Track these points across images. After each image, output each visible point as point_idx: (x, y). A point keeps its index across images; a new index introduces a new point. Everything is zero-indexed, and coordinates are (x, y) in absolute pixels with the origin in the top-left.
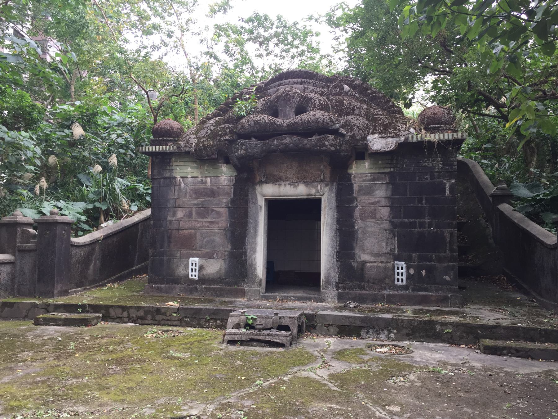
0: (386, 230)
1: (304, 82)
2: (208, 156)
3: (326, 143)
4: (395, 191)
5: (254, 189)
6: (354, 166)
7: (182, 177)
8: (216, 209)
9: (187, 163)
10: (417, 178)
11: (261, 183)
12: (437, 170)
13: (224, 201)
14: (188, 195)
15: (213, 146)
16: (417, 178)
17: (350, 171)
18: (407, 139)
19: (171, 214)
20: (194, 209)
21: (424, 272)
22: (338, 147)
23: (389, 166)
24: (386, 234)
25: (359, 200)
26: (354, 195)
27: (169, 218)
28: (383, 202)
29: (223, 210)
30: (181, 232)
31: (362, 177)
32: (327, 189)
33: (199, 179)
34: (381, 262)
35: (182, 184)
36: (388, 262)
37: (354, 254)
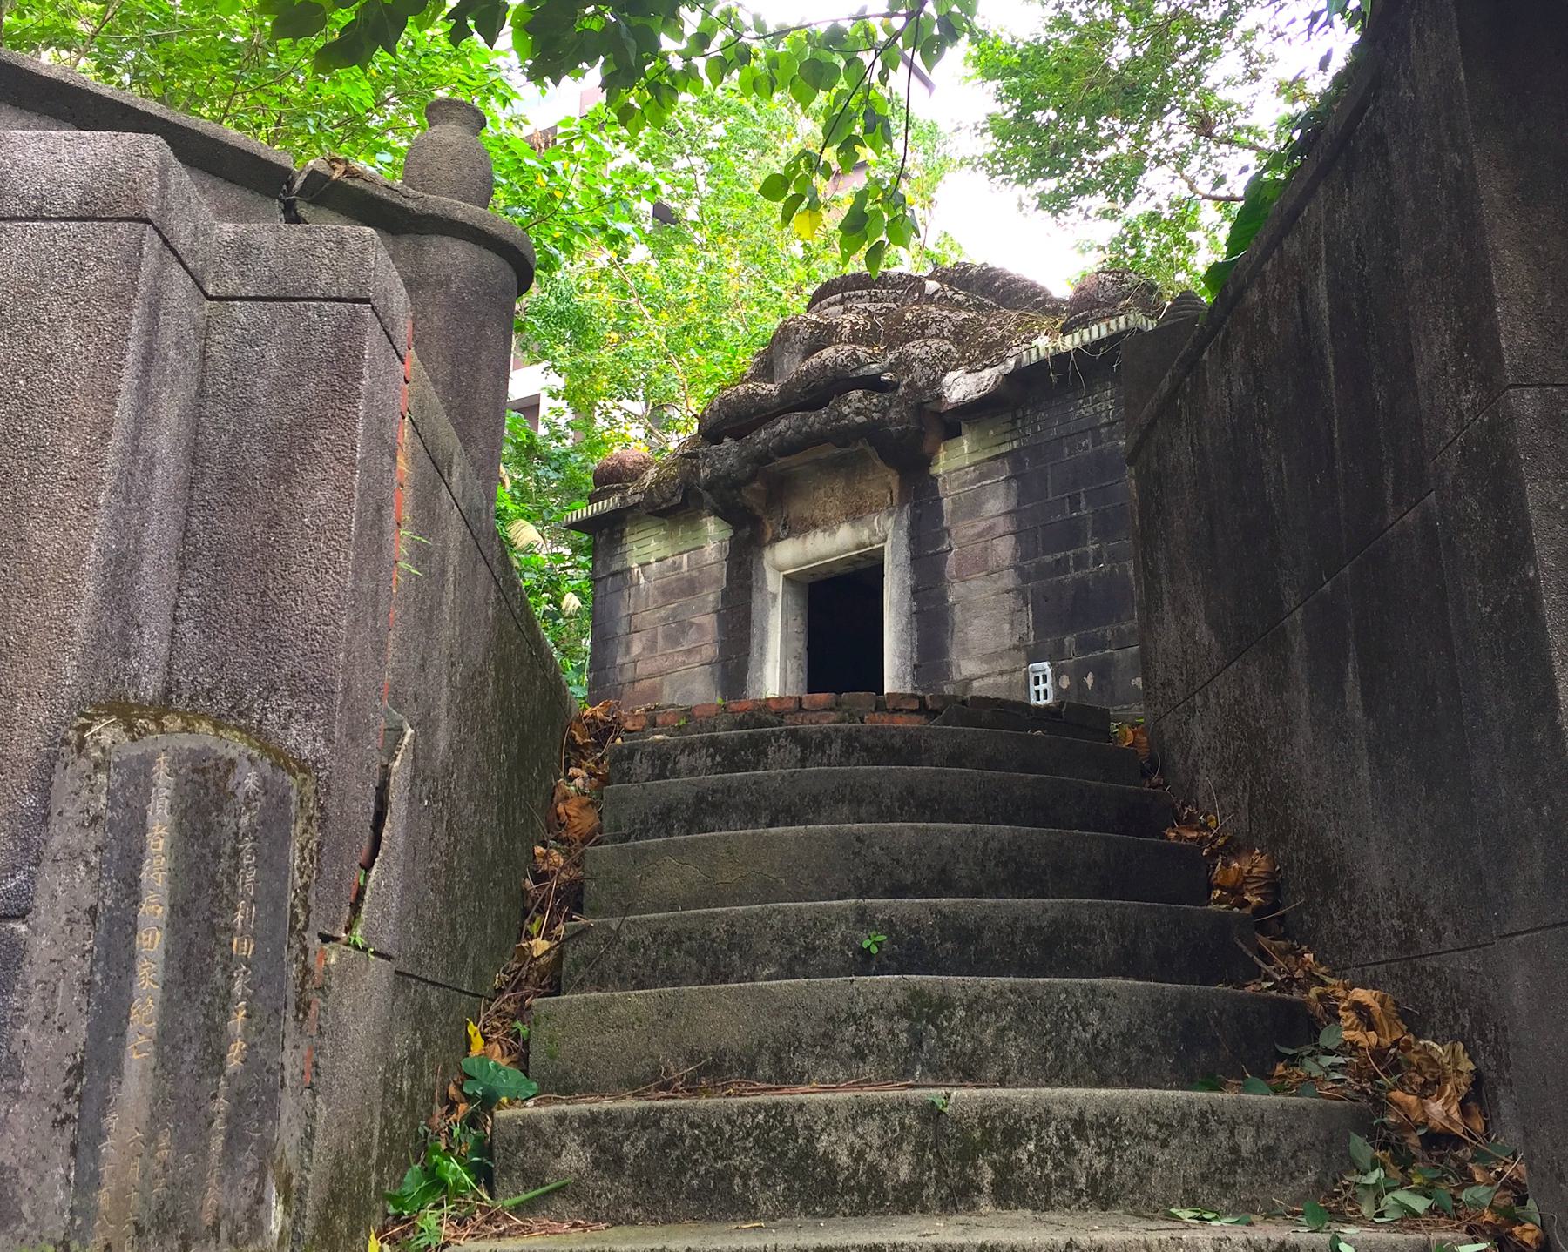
0: (1008, 592)
1: (850, 298)
2: (665, 501)
3: (846, 410)
4: (1022, 497)
5: (762, 557)
6: (942, 455)
7: (640, 565)
8: (696, 620)
9: (649, 533)
10: (1066, 450)
11: (776, 539)
12: (1105, 420)
13: (711, 598)
14: (651, 601)
15: (673, 478)
16: (1066, 450)
17: (934, 470)
18: (1018, 363)
19: (622, 649)
20: (660, 630)
21: (1089, 680)
22: (875, 415)
23: (1008, 437)
24: (1009, 602)
25: (953, 532)
26: (945, 524)
27: (619, 661)
28: (1003, 525)
29: (709, 621)
30: (638, 686)
31: (957, 478)
32: (890, 523)
33: (670, 560)
34: (1001, 673)
35: (642, 580)
36: (1015, 671)
37: (948, 665)
